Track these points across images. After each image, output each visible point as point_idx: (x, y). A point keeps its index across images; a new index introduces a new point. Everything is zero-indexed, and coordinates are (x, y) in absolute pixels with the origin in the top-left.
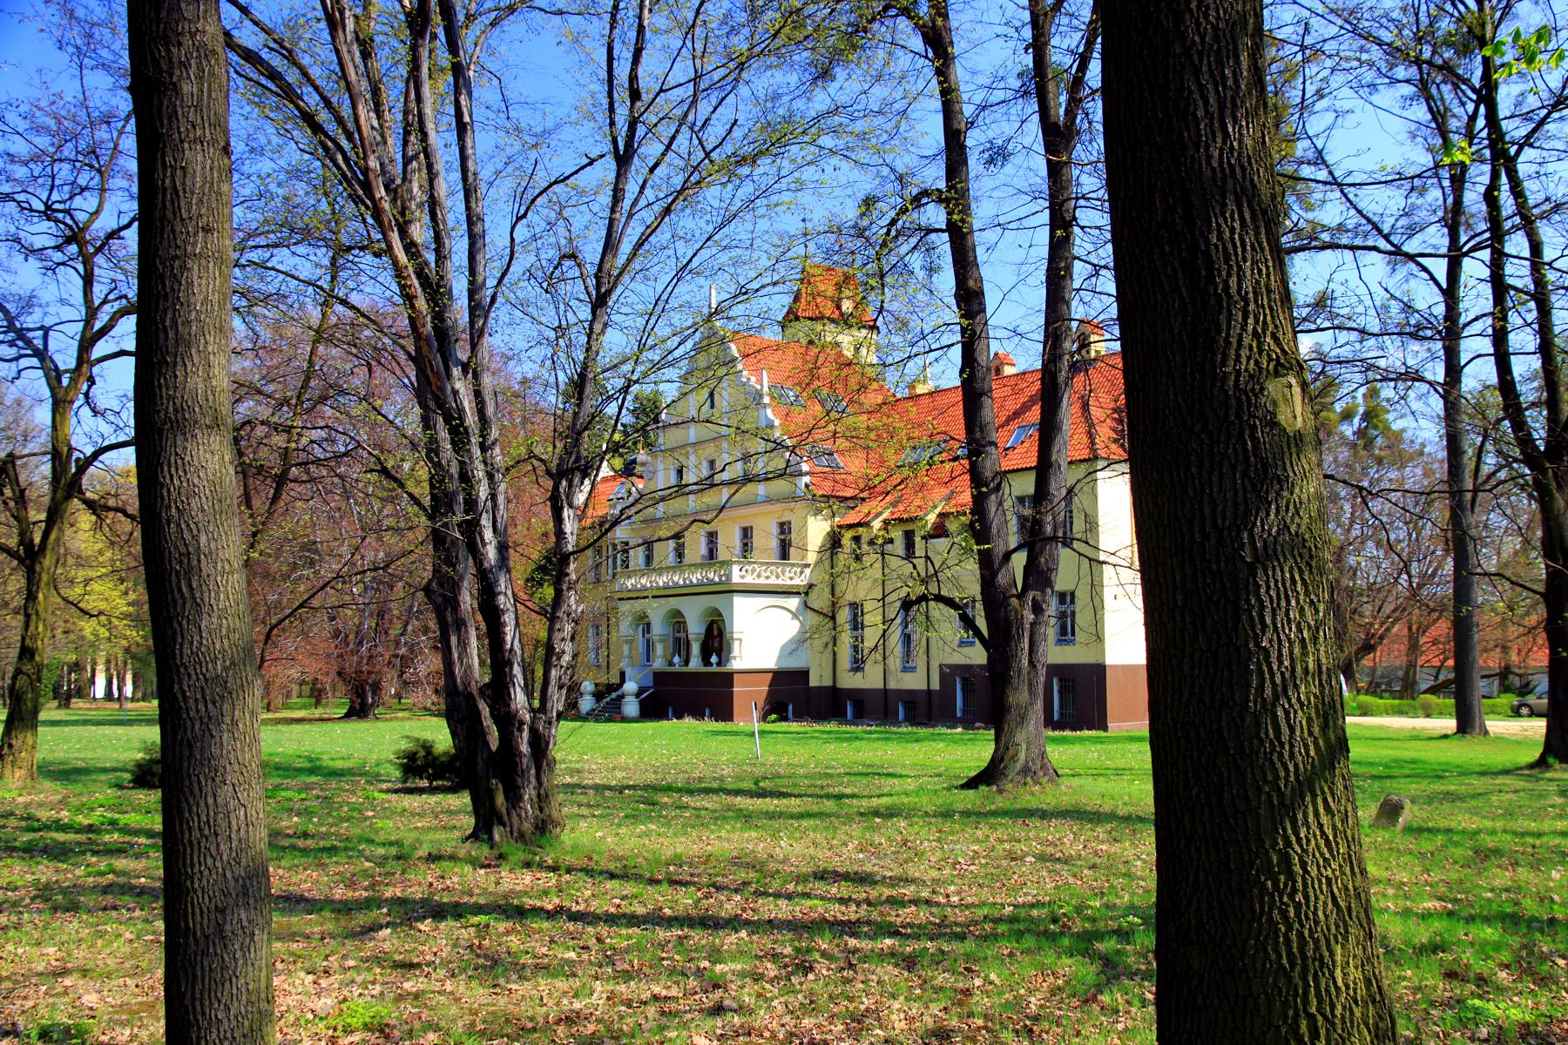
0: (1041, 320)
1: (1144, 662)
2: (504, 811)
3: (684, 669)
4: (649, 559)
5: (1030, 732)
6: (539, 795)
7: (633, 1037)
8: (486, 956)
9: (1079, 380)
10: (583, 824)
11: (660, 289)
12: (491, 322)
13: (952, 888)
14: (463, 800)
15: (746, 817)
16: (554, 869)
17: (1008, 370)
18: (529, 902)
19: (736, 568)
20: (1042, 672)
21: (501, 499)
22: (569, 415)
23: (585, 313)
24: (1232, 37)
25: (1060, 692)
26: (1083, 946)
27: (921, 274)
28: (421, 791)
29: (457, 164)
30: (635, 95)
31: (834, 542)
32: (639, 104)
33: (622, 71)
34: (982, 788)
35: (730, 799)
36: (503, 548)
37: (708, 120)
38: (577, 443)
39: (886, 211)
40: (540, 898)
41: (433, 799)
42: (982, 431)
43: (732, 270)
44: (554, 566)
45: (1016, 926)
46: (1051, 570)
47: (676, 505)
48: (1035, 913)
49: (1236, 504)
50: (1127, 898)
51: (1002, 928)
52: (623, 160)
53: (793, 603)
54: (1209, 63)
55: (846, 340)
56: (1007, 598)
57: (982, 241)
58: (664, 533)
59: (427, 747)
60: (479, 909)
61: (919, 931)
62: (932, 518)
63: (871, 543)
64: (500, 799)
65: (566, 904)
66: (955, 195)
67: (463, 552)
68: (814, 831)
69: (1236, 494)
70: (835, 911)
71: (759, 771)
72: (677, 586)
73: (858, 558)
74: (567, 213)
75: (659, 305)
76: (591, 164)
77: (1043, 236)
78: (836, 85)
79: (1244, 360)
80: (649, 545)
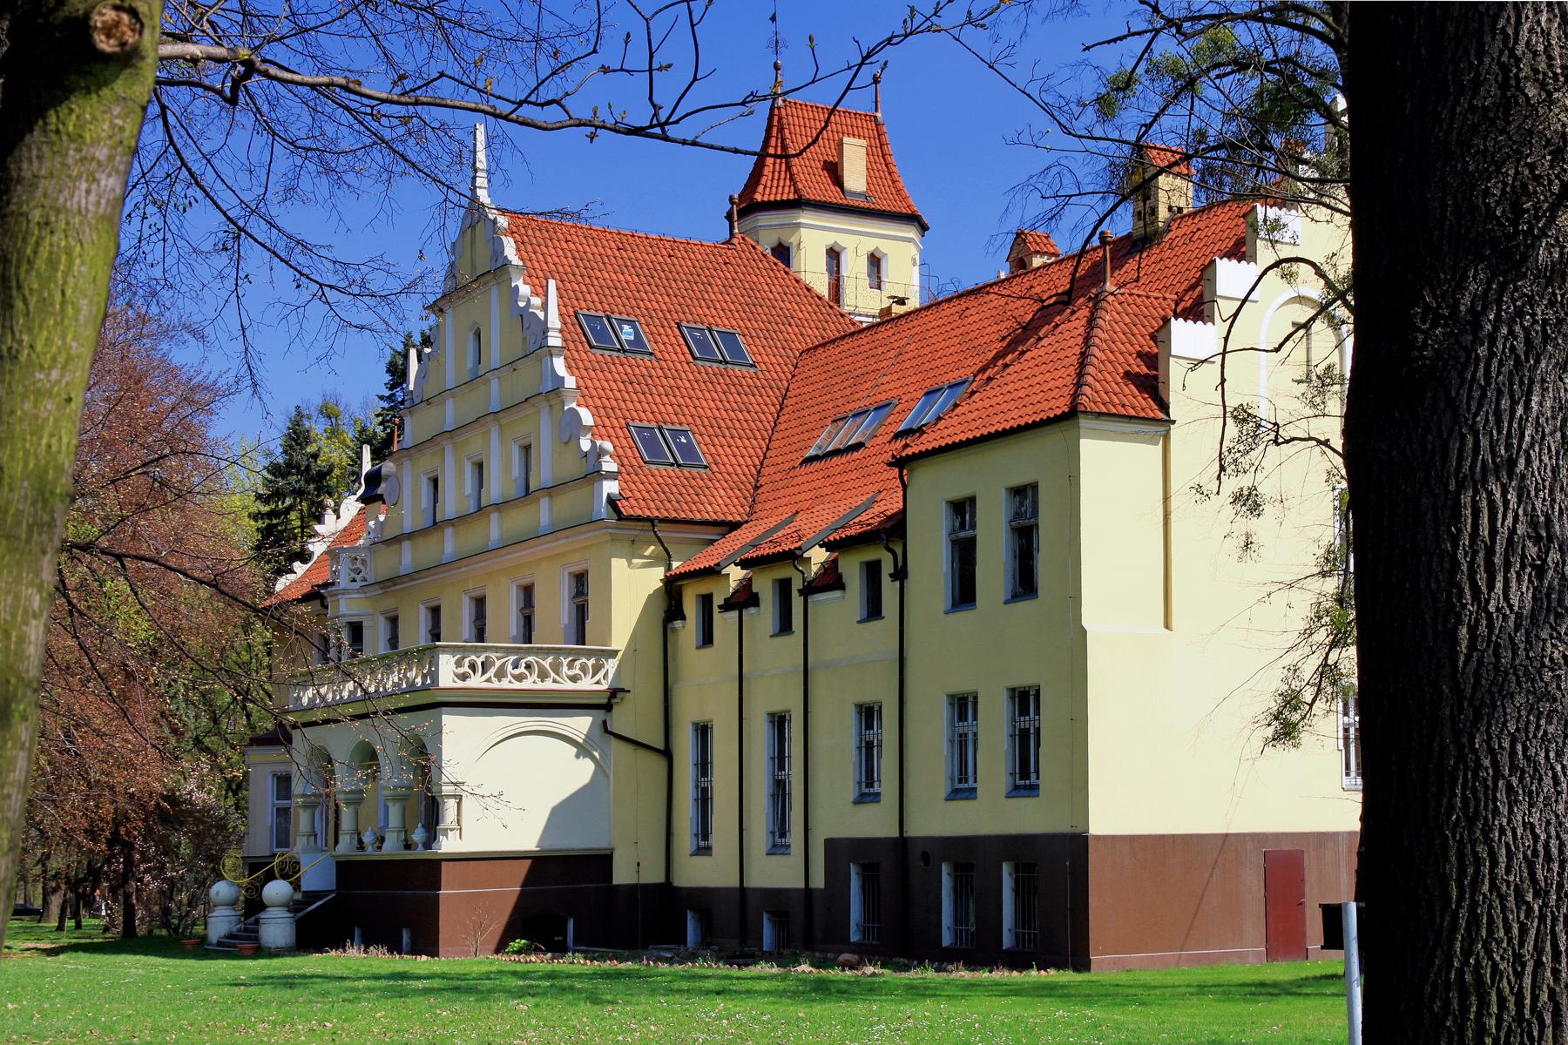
1: (1356, 826)
53: (580, 725)
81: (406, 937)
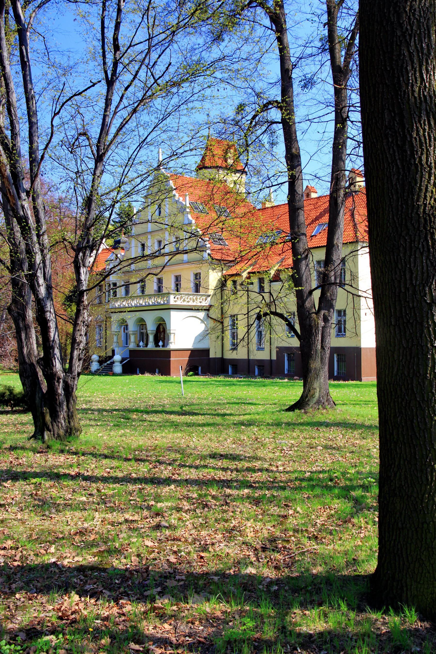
0: (330, 170)
2: (49, 423)
3: (146, 349)
4: (127, 292)
5: (321, 382)
6: (68, 416)
7: (114, 541)
8: (39, 500)
9: (349, 202)
10: (92, 430)
11: (131, 152)
12: (42, 168)
13: (280, 463)
14: (28, 417)
15: (176, 426)
16: (76, 453)
17: (313, 195)
18: (62, 471)
19: (172, 297)
20: (328, 352)
21: (48, 262)
22: (83, 219)
23: (91, 164)
24: (427, 26)
25: (338, 361)
26: (344, 493)
27: (267, 146)
28: (7, 413)
29: (22, 83)
30: (116, 47)
31: (222, 284)
32: (118, 52)
33: (109, 34)
34: (297, 411)
35: (167, 416)
36: (49, 288)
37: (155, 62)
38: (87, 234)
39: (250, 111)
40: (68, 468)
41: (13, 417)
42: (298, 228)
43: (169, 143)
44: (76, 297)
45: (312, 483)
46: (332, 300)
47: (141, 265)
48: (321, 476)
49: (423, 273)
50: (368, 468)
51: (304, 484)
52: (110, 83)
53: (202, 315)
54: (415, 40)
55: (231, 178)
56: (310, 314)
57: (299, 128)
58: (133, 280)
59: (11, 390)
60: (36, 475)
61: (263, 485)
62: (272, 272)
63: (242, 284)
64: (48, 418)
65: (82, 472)
66: (286, 104)
67: (27, 289)
68: (210, 433)
69: (423, 268)
70: (220, 475)
71: (183, 402)
72: (141, 306)
73: (235, 293)
74: (82, 110)
75: (130, 162)
76: (93, 86)
77: (331, 127)
78: (223, 44)
79: (428, 199)
80: (127, 286)
81: (157, 371)
